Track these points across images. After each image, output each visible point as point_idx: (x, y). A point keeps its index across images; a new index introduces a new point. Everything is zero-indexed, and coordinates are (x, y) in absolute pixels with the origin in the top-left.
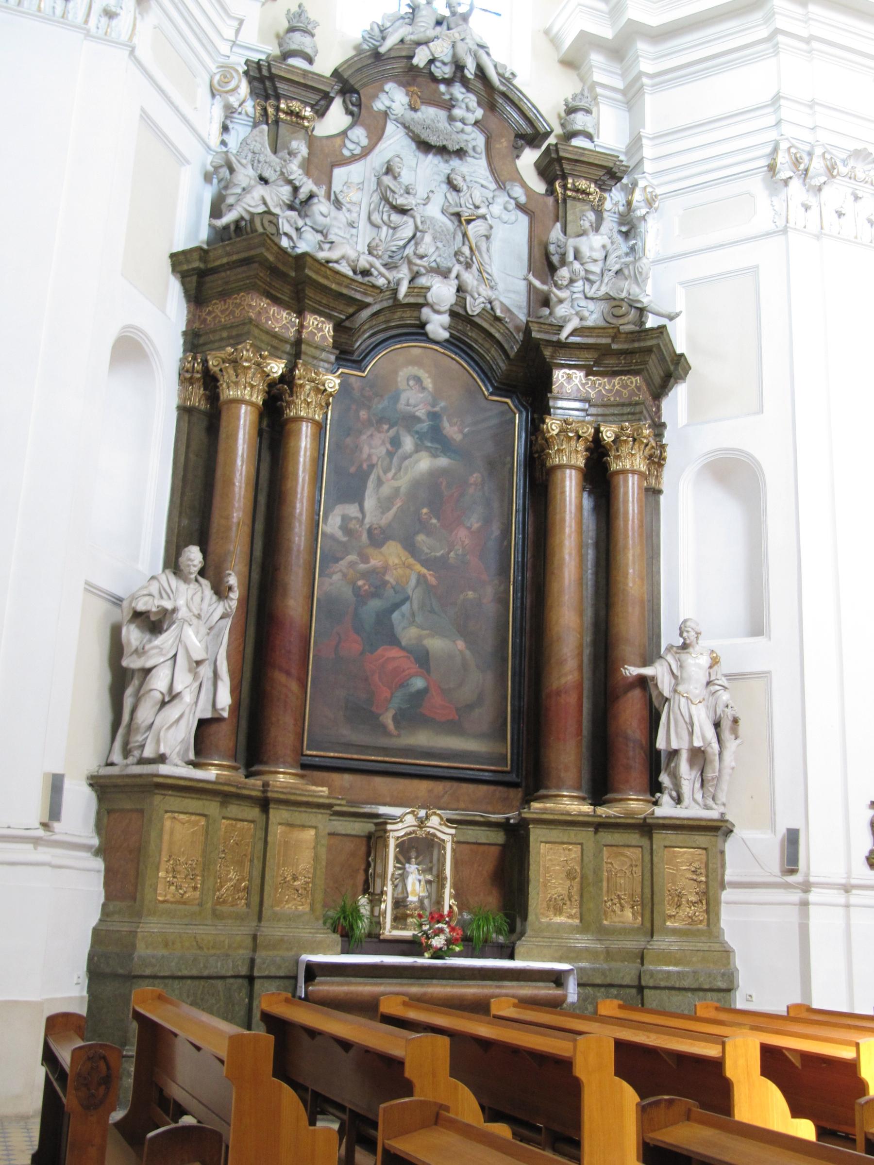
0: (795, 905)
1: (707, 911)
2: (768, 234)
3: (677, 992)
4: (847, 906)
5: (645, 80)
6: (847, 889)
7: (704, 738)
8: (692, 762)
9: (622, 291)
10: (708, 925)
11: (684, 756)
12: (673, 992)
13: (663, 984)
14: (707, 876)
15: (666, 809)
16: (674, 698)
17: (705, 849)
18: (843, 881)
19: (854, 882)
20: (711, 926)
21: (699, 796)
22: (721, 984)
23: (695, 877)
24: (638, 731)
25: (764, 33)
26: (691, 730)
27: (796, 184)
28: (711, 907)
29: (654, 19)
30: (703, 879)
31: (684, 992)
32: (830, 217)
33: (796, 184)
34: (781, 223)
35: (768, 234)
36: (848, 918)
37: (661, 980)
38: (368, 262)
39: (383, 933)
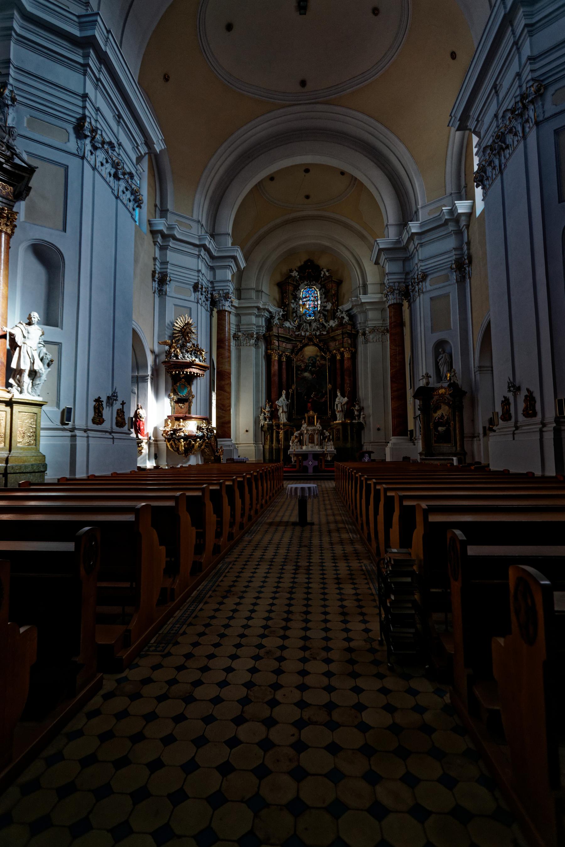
0: (68, 437)
1: (35, 440)
2: (74, 154)
3: (23, 474)
4: (88, 437)
5: (169, 247)
6: (85, 431)
7: (39, 366)
8: (30, 375)
9: (4, 139)
10: (36, 445)
11: (26, 374)
12: (22, 474)
13: (17, 471)
14: (36, 425)
15: (17, 396)
16: (24, 346)
17: (36, 413)
18: (85, 428)
19: (89, 428)
20: (37, 446)
21: (30, 390)
22: (42, 469)
23: (31, 425)
24: (3, 358)
25: (81, 60)
26: (32, 362)
27: (88, 141)
28: (37, 438)
29: (178, 236)
30: (34, 426)
31: (26, 474)
32: (98, 164)
33: (88, 141)
34: (82, 155)
35: (74, 154)
36: (88, 441)
37: (17, 470)
38: (427, 506)
39: (222, 368)
